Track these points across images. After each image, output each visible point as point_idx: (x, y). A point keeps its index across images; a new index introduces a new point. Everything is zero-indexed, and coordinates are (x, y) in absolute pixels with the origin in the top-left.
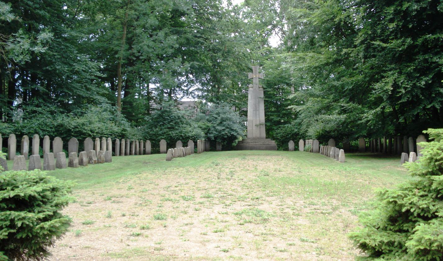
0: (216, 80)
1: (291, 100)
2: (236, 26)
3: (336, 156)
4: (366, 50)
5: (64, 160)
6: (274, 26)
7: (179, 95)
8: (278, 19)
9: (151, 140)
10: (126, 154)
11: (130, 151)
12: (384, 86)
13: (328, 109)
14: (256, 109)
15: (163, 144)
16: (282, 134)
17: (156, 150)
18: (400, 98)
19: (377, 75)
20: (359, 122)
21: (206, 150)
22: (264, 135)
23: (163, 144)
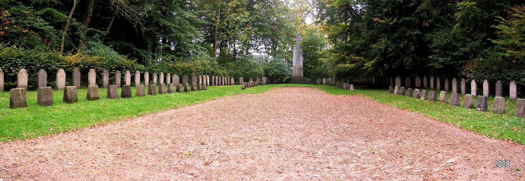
0: (275, 43)
1: (320, 55)
2: (286, 10)
3: (348, 88)
4: (368, 24)
5: (189, 88)
6: (309, 12)
7: (251, 51)
8: (311, 8)
9: (234, 77)
10: (218, 85)
11: (215, 82)
12: (380, 45)
13: (343, 60)
14: (298, 59)
15: (241, 79)
16: (311, 76)
17: (237, 82)
18: (388, 54)
19: (374, 40)
20: (363, 68)
21: (267, 83)
22: (302, 75)
23: (241, 79)
